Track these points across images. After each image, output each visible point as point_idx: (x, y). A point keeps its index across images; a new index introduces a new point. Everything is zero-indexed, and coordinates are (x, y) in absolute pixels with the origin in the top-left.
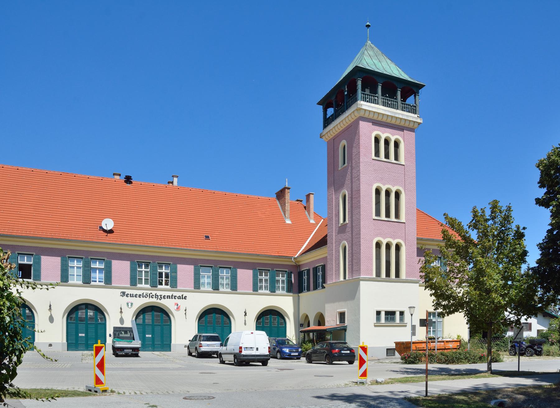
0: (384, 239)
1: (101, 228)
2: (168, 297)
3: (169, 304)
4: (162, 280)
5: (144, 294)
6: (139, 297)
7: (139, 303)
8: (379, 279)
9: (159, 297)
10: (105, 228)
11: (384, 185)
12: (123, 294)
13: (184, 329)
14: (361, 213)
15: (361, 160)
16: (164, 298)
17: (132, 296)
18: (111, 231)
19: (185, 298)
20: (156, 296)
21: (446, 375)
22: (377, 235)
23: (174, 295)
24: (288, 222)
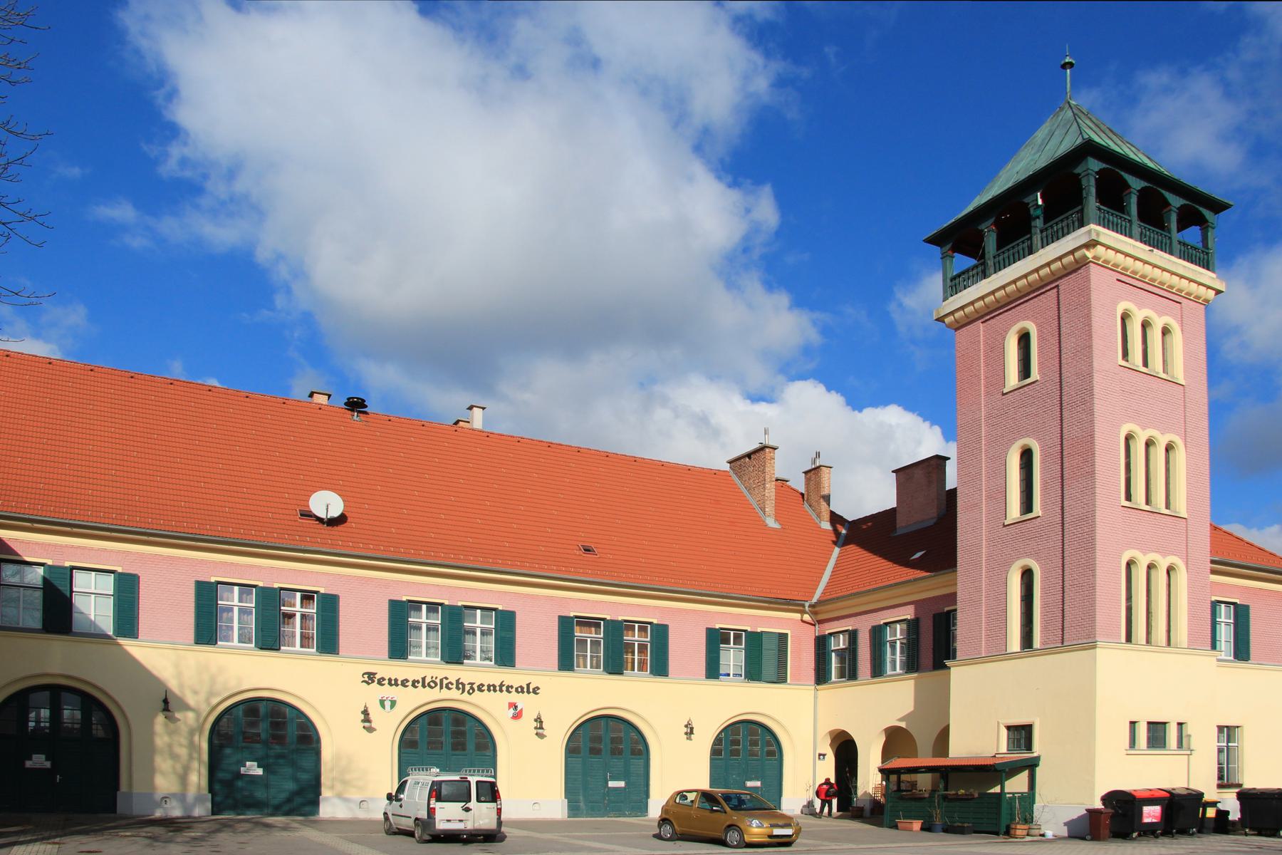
0: (1145, 554)
1: (308, 515)
2: (492, 688)
3: (489, 710)
6: (414, 685)
7: (413, 701)
8: (1027, 652)
10: (322, 515)
11: (1144, 428)
12: (370, 677)
14: (1097, 490)
15: (1095, 364)
17: (393, 683)
18: (341, 519)
19: (536, 691)
20: (460, 685)
21: (36, 841)
22: (1129, 546)
23: (506, 683)
24: (771, 523)
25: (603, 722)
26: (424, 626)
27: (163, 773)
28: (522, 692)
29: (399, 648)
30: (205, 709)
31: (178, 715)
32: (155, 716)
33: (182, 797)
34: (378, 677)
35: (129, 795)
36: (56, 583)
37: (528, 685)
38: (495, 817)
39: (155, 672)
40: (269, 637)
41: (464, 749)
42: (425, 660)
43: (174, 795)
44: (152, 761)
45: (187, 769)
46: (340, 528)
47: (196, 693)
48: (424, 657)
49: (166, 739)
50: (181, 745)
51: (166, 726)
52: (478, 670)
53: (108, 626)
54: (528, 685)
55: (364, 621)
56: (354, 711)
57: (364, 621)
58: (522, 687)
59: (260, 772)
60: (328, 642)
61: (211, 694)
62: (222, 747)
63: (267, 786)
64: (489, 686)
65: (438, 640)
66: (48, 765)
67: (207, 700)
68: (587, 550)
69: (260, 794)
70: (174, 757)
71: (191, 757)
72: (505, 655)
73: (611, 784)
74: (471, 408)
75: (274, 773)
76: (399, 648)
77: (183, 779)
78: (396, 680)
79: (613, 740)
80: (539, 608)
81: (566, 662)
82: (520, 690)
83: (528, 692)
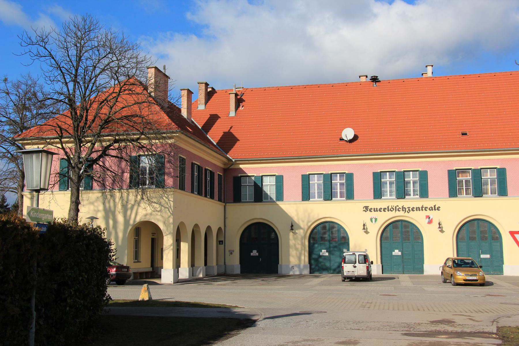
1: (342, 139)
2: (418, 209)
3: (418, 219)
4: (340, 189)
5: (390, 207)
6: (384, 211)
9: (424, 209)
12: (366, 209)
13: (438, 250)
16: (413, 210)
17: (376, 210)
18: (356, 138)
19: (438, 209)
25: (476, 222)
26: (388, 182)
27: (293, 256)
28: (432, 210)
29: (378, 194)
30: (306, 227)
31: (297, 231)
32: (289, 233)
33: (299, 266)
34: (369, 208)
35: (281, 265)
36: (257, 182)
37: (435, 206)
38: (366, 270)
39: (289, 214)
40: (329, 195)
41: (409, 240)
42: (389, 200)
43: (296, 265)
44: (289, 251)
45: (300, 254)
46: (355, 143)
47: (303, 221)
48: (388, 197)
49: (294, 242)
50: (298, 244)
51: (293, 236)
52: (413, 201)
53: (274, 197)
54: (435, 206)
55: (364, 184)
56: (361, 224)
57: (364, 184)
58: (432, 207)
59: (327, 254)
60: (350, 195)
61: (309, 221)
62: (314, 244)
63: (330, 260)
64: (417, 208)
65: (394, 189)
66: (257, 254)
67: (307, 224)
68: (464, 134)
69: (328, 264)
70: (296, 249)
71: (302, 249)
72: (424, 193)
73: (482, 256)
74: (426, 67)
75: (333, 254)
76: (378, 194)
77: (299, 259)
78: (377, 209)
79: (482, 232)
80: (437, 168)
81: (453, 192)
82: (431, 209)
83: (435, 210)
